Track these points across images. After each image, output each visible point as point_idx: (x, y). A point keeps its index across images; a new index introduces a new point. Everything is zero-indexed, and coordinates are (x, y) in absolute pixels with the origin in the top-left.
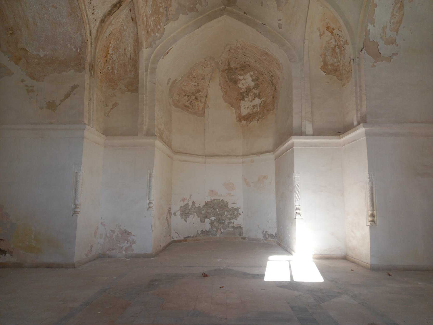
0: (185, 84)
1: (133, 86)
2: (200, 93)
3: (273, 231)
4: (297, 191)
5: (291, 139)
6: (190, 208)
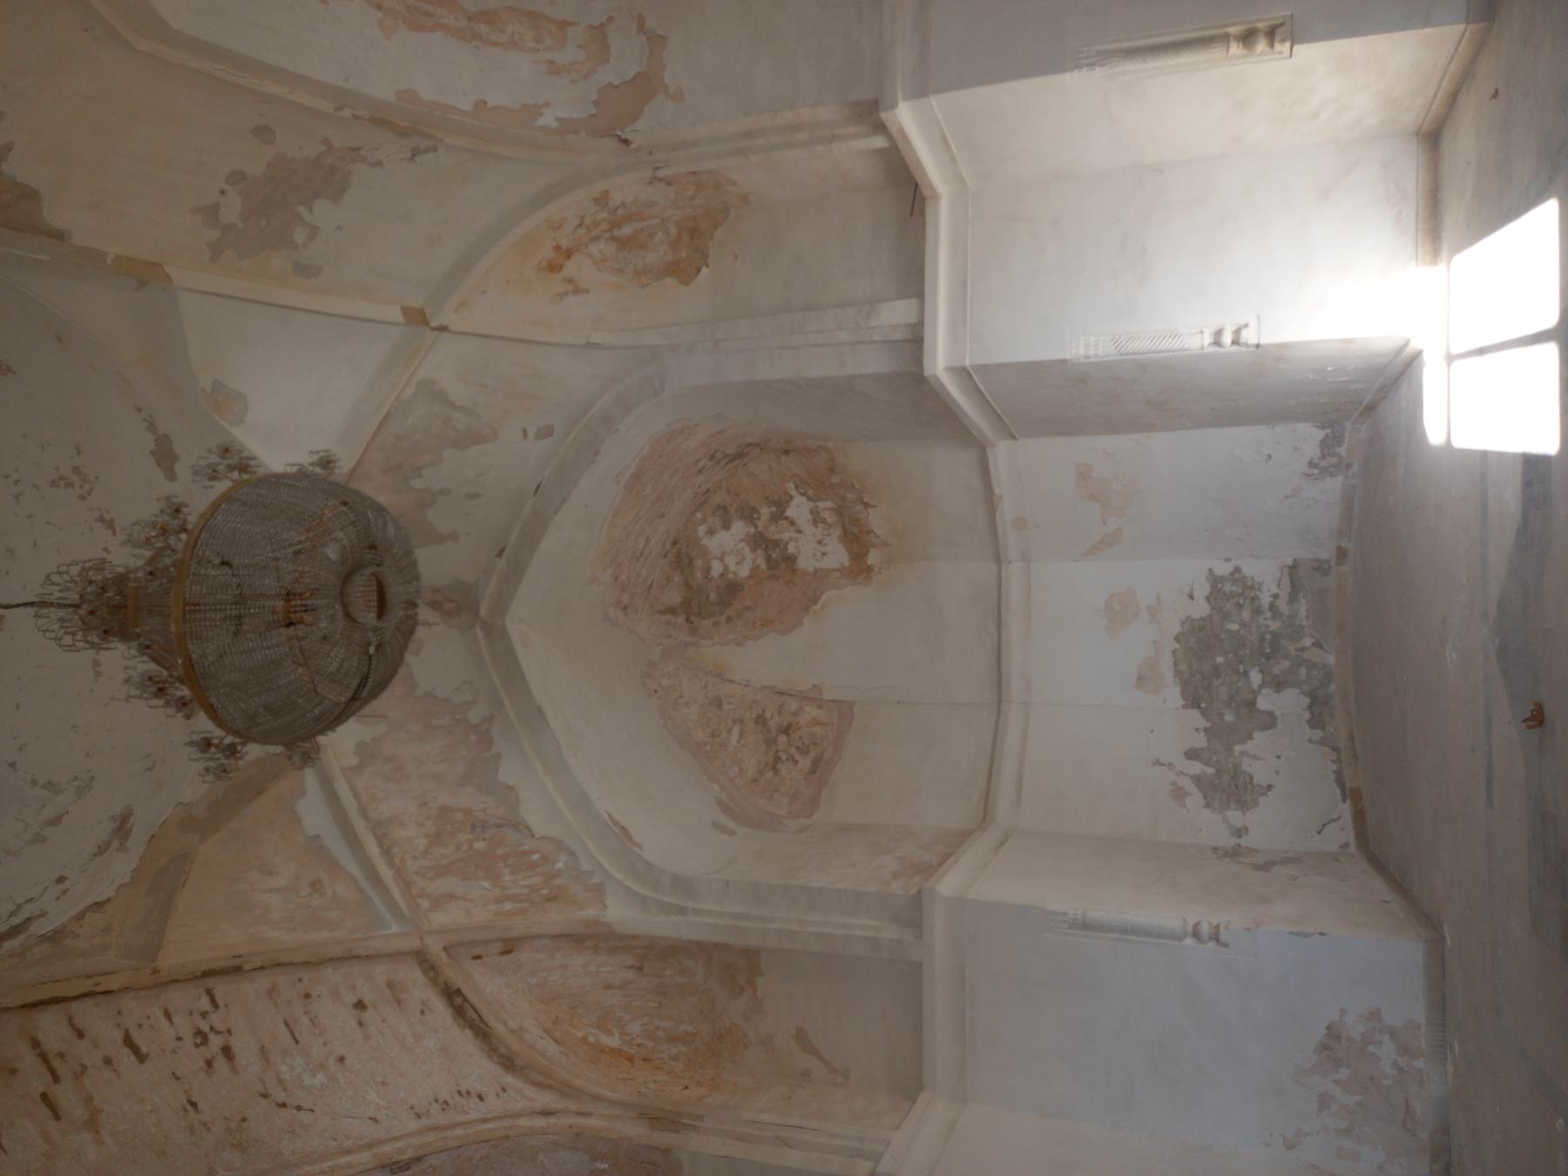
0: (736, 769)
1: (736, 965)
2: (768, 715)
3: (1310, 437)
4: (1142, 345)
5: (935, 377)
6: (1211, 770)
